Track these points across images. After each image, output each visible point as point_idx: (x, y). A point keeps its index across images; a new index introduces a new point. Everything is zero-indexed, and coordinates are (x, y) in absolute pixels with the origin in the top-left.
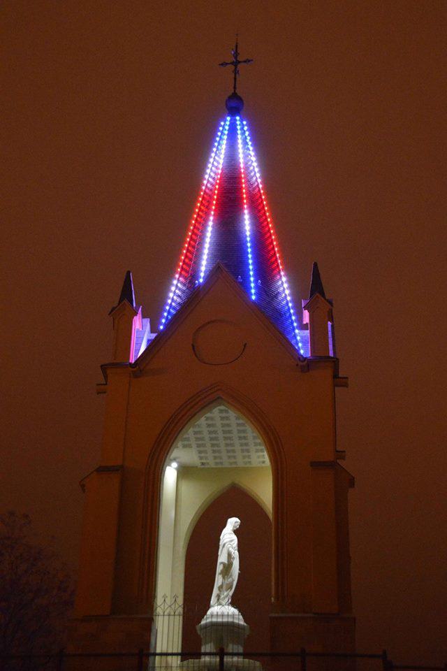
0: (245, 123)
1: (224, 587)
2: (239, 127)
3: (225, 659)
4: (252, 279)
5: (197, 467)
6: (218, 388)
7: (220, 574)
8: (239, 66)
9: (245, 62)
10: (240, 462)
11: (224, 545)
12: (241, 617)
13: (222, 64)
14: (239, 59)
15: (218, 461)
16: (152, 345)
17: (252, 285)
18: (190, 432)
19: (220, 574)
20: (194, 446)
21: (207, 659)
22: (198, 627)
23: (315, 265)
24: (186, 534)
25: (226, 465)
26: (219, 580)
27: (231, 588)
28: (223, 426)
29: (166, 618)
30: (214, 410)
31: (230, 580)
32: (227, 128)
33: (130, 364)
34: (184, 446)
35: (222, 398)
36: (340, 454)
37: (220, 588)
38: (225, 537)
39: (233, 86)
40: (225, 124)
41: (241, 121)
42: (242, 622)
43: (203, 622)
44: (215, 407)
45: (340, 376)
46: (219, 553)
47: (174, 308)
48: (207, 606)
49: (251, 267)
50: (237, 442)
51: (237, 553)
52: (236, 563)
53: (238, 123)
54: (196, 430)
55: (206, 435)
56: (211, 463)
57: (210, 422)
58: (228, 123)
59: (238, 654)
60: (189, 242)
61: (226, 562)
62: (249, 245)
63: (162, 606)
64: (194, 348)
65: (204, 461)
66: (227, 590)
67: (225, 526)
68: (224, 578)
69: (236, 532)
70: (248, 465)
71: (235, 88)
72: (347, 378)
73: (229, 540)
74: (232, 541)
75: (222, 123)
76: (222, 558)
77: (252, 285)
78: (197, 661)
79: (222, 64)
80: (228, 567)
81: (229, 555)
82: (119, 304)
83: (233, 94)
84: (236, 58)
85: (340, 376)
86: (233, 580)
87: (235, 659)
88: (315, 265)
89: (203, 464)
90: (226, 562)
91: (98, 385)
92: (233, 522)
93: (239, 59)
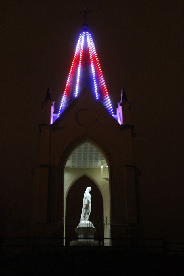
10: (88, 166)
11: (86, 197)
12: (93, 225)
18: (76, 151)
19: (84, 208)
21: (80, 240)
22: (76, 229)
26: (84, 211)
27: (89, 214)
29: (108, 225)
31: (88, 211)
37: (85, 214)
42: (93, 227)
43: (78, 227)
48: (79, 220)
54: (79, 149)
56: (76, 166)
59: (92, 239)
61: (87, 204)
63: (107, 221)
65: (73, 165)
66: (87, 215)
68: (86, 210)
69: (90, 192)
70: (90, 167)
76: (85, 202)
78: (75, 241)
80: (87, 206)
81: (88, 201)
86: (89, 211)
87: (91, 241)
92: (89, 189)
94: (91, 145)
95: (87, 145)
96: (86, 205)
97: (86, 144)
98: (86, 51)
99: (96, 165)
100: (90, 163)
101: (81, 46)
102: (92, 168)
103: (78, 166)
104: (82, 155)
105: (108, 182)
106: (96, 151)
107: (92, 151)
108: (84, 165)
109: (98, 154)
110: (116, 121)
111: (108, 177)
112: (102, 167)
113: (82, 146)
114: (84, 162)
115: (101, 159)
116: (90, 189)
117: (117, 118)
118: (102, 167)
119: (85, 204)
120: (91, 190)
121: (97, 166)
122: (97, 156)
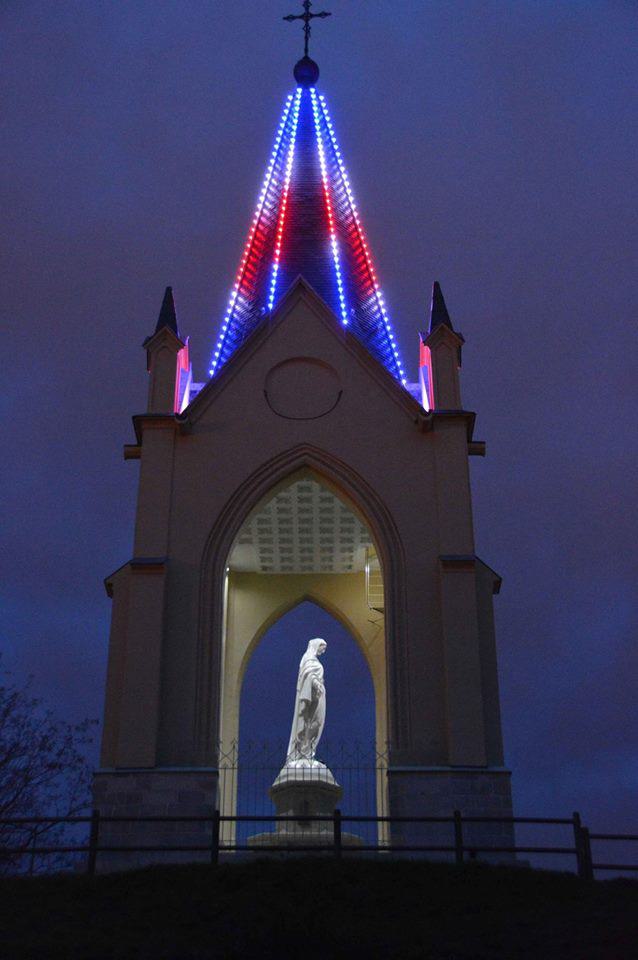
0: (322, 98)
1: (307, 733)
2: (314, 102)
3: (331, 833)
4: (343, 306)
5: (255, 573)
6: (304, 451)
7: (300, 715)
9: (320, 15)
10: (317, 570)
11: (307, 674)
15: (286, 564)
16: (197, 400)
17: (344, 314)
18: (253, 524)
19: (300, 715)
20: (255, 540)
23: (437, 285)
24: (241, 669)
25: (297, 570)
26: (298, 725)
28: (301, 511)
30: (291, 488)
32: (298, 103)
33: (177, 414)
34: (243, 542)
35: (308, 466)
37: (301, 735)
38: (308, 664)
40: (294, 100)
41: (318, 95)
42: (276, 783)
43: (276, 783)
44: (293, 483)
46: (298, 688)
47: (228, 347)
48: (282, 761)
49: (341, 290)
50: (317, 536)
51: (323, 687)
52: (322, 701)
53: (313, 96)
56: (276, 566)
57: (283, 505)
58: (299, 96)
62: (337, 267)
64: (266, 396)
65: (267, 564)
67: (305, 651)
68: (306, 721)
69: (321, 658)
70: (327, 572)
71: (306, 50)
72: (484, 443)
73: (311, 669)
74: (316, 670)
75: (290, 98)
76: (303, 693)
77: (344, 314)
80: (311, 706)
81: (314, 689)
82: (157, 332)
84: (307, 8)
88: (437, 285)
89: (264, 568)
90: (310, 699)
91: (126, 446)
92: (316, 645)
93: (312, 10)
94: (322, 490)
95: (309, 489)
96: (306, 701)
97: (304, 483)
98: (382, 765)
99: (348, 563)
100: (328, 554)
101: (281, 182)
102: (332, 572)
103: (283, 568)
104: (296, 526)
105: (380, 616)
106: (344, 511)
107: (329, 510)
108: (307, 564)
109: (351, 521)
110: (413, 401)
111: (381, 604)
112: (367, 569)
113: (292, 492)
114: (302, 551)
115: (363, 540)
116: (321, 645)
117: (420, 394)
118: (367, 569)
119: (301, 698)
120: (326, 649)
121: (350, 567)
122: (350, 531)
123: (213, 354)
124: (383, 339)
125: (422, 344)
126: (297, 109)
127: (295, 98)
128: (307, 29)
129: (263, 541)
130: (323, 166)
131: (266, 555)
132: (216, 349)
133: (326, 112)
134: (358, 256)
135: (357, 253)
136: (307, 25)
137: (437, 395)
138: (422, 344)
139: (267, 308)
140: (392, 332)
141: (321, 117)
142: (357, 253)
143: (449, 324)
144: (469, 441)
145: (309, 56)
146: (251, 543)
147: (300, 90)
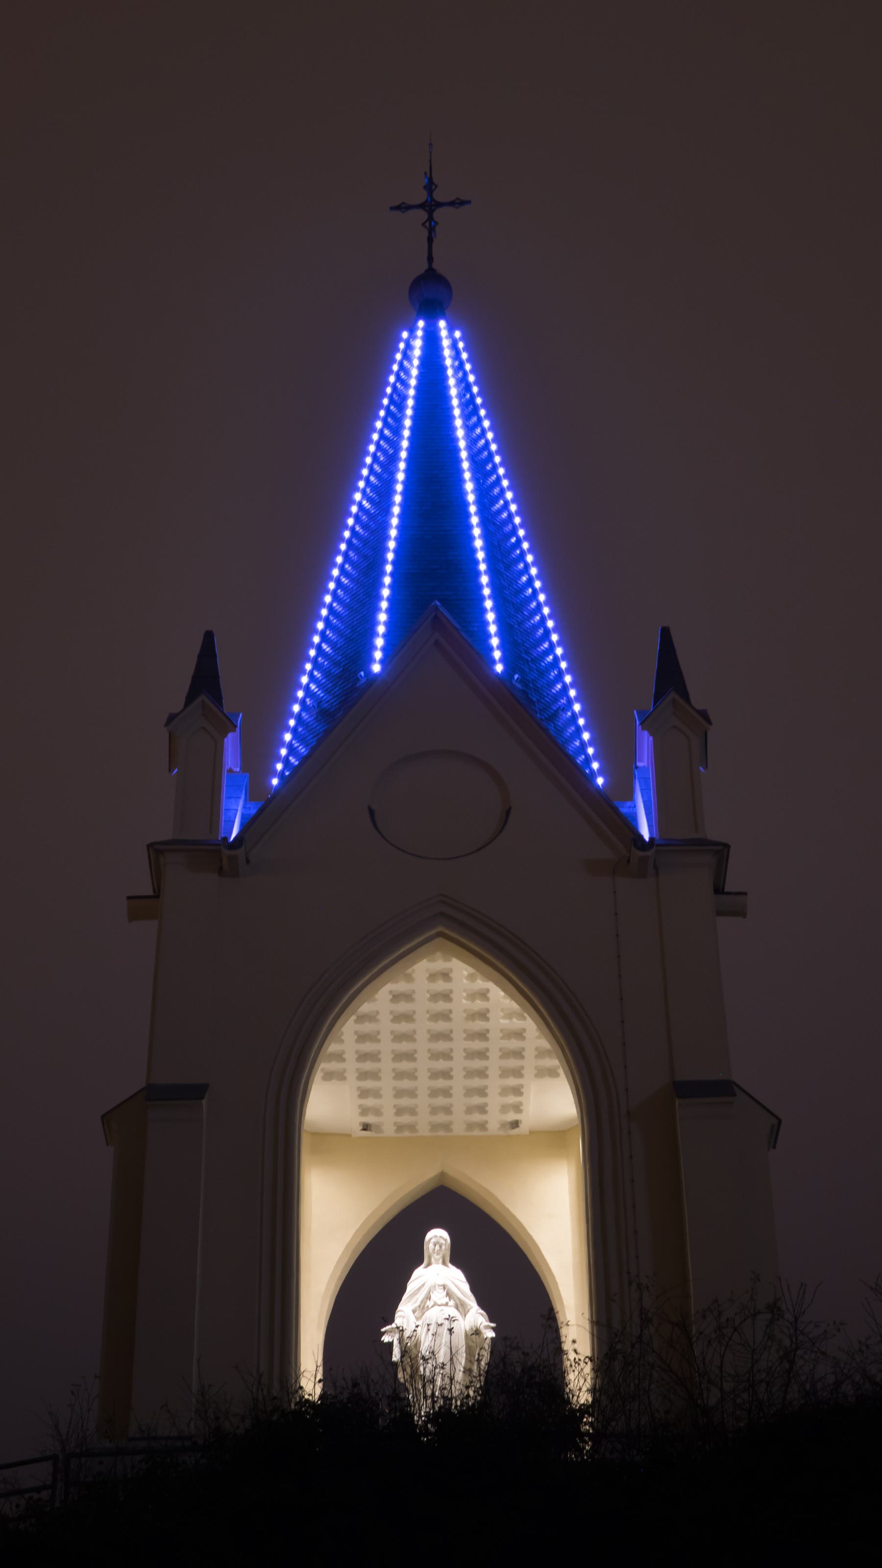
0: (457, 334)
2: (446, 343)
5: (350, 1135)
8: (438, 214)
13: (398, 208)
14: (438, 196)
20: (351, 1076)
34: (329, 1076)
36: (446, 1365)
39: (426, 254)
41: (451, 329)
45: (727, 890)
53: (444, 333)
55: (386, 1047)
60: (335, 591)
65: (370, 1119)
71: (430, 259)
72: (745, 894)
75: (405, 335)
79: (398, 208)
83: (427, 271)
85: (727, 890)
89: (366, 1127)
95: (446, 976)
97: (439, 964)
99: (511, 1116)
103: (400, 1128)
121: (515, 1124)
123: (275, 767)
124: (579, 754)
125: (639, 728)
126: (417, 352)
127: (412, 335)
128: (430, 186)
129: (363, 1075)
130: (460, 433)
131: (370, 1102)
132: (278, 758)
133: (464, 356)
134: (500, 512)
135: (497, 506)
136: (430, 218)
137: (659, 820)
138: (639, 728)
139: (369, 672)
140: (491, 428)
141: (460, 374)
142: (497, 506)
143: (685, 696)
144: (719, 890)
145: (434, 266)
146: (344, 1078)
147: (421, 324)
